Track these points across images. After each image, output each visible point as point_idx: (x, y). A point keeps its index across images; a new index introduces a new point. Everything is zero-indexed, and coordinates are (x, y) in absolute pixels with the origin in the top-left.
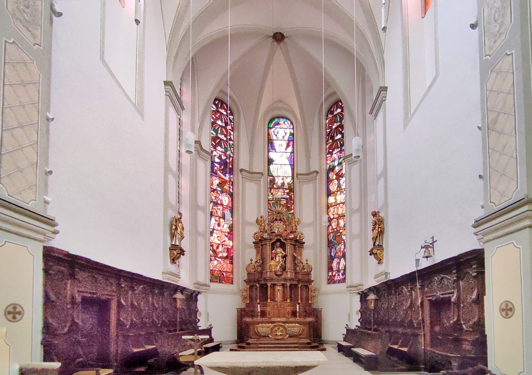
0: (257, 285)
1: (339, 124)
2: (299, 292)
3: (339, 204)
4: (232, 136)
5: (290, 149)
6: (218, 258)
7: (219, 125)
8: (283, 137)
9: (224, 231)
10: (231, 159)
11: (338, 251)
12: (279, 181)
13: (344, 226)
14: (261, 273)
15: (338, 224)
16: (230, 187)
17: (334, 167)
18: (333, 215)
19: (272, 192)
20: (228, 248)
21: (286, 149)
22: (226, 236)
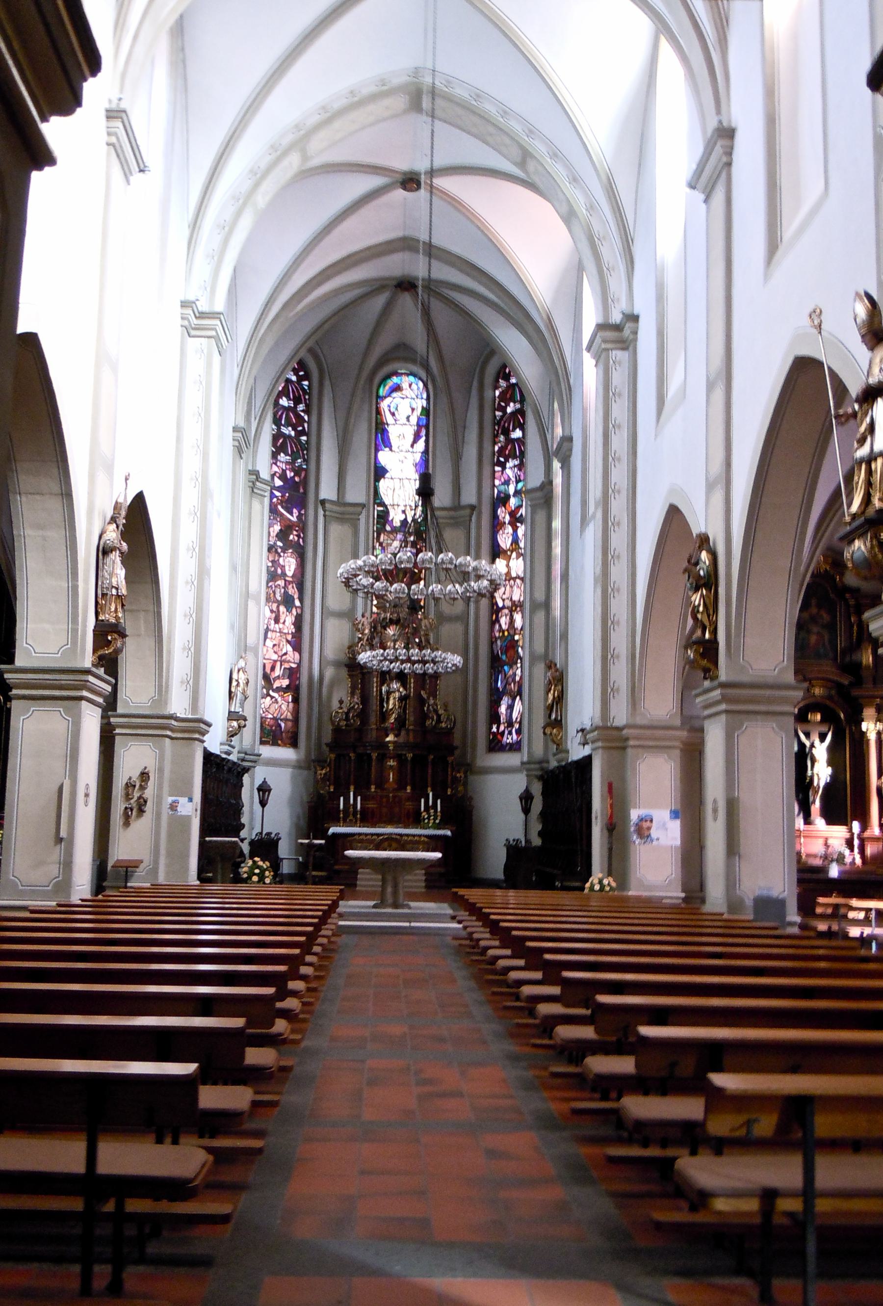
0: (352, 755)
1: (518, 406)
2: (430, 771)
3: (514, 579)
4: (306, 425)
5: (421, 445)
6: (273, 691)
7: (283, 407)
8: (408, 418)
9: (286, 631)
10: (303, 475)
11: (510, 680)
12: (396, 517)
13: (522, 629)
14: (361, 731)
15: (512, 621)
16: (298, 536)
17: (507, 497)
18: (503, 600)
19: (382, 539)
20: (291, 669)
21: (412, 446)
22: (288, 641)
